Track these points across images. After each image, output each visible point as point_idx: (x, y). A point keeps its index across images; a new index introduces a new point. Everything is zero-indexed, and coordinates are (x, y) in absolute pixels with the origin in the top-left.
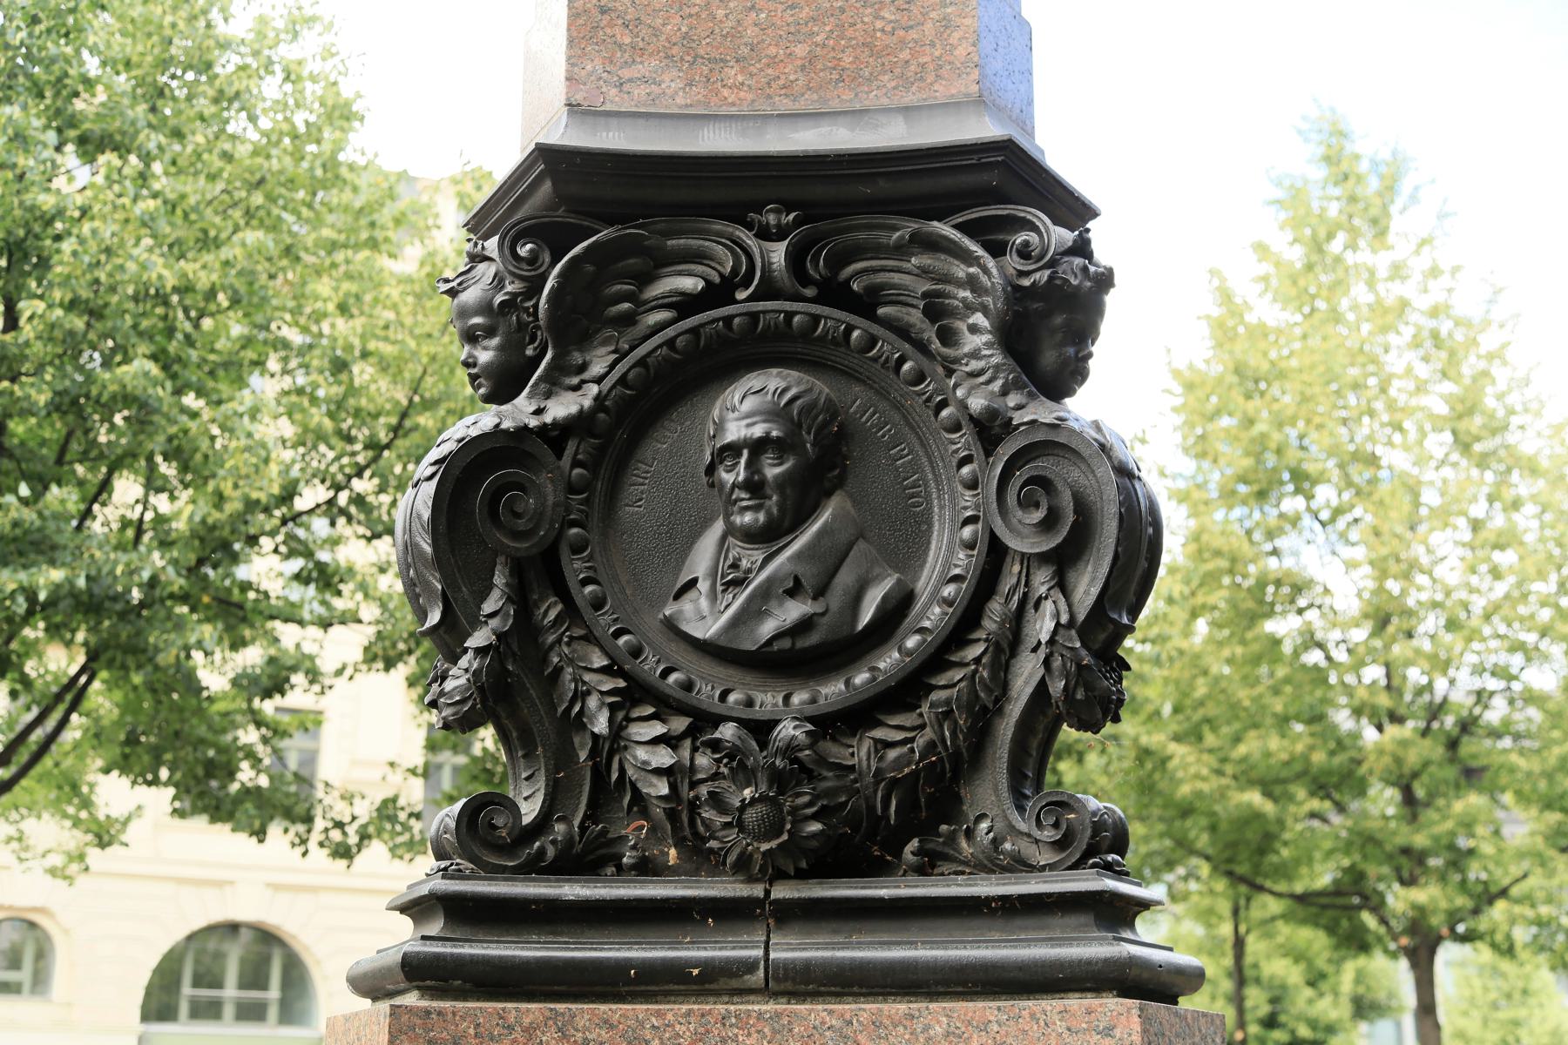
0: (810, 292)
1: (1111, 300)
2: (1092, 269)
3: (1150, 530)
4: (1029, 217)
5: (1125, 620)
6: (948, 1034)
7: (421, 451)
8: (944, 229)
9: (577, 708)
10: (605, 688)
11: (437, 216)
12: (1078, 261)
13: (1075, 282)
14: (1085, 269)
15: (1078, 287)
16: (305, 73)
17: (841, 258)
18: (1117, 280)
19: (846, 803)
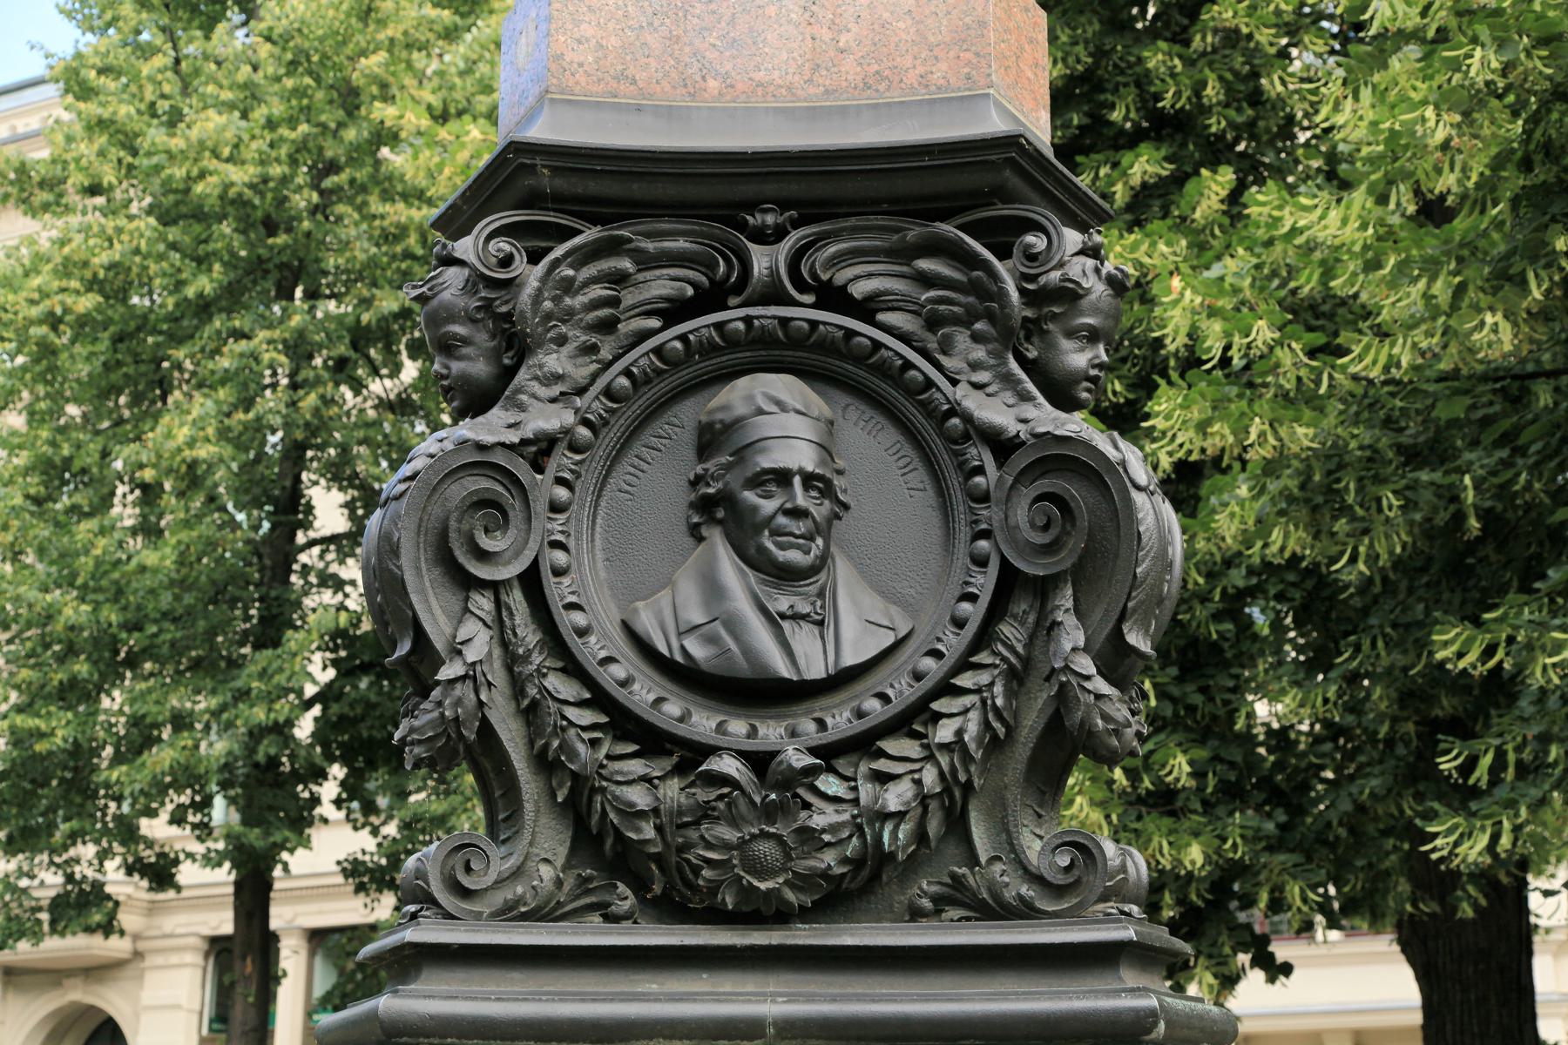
0: (809, 299)
9: (556, 743)
10: (584, 723)
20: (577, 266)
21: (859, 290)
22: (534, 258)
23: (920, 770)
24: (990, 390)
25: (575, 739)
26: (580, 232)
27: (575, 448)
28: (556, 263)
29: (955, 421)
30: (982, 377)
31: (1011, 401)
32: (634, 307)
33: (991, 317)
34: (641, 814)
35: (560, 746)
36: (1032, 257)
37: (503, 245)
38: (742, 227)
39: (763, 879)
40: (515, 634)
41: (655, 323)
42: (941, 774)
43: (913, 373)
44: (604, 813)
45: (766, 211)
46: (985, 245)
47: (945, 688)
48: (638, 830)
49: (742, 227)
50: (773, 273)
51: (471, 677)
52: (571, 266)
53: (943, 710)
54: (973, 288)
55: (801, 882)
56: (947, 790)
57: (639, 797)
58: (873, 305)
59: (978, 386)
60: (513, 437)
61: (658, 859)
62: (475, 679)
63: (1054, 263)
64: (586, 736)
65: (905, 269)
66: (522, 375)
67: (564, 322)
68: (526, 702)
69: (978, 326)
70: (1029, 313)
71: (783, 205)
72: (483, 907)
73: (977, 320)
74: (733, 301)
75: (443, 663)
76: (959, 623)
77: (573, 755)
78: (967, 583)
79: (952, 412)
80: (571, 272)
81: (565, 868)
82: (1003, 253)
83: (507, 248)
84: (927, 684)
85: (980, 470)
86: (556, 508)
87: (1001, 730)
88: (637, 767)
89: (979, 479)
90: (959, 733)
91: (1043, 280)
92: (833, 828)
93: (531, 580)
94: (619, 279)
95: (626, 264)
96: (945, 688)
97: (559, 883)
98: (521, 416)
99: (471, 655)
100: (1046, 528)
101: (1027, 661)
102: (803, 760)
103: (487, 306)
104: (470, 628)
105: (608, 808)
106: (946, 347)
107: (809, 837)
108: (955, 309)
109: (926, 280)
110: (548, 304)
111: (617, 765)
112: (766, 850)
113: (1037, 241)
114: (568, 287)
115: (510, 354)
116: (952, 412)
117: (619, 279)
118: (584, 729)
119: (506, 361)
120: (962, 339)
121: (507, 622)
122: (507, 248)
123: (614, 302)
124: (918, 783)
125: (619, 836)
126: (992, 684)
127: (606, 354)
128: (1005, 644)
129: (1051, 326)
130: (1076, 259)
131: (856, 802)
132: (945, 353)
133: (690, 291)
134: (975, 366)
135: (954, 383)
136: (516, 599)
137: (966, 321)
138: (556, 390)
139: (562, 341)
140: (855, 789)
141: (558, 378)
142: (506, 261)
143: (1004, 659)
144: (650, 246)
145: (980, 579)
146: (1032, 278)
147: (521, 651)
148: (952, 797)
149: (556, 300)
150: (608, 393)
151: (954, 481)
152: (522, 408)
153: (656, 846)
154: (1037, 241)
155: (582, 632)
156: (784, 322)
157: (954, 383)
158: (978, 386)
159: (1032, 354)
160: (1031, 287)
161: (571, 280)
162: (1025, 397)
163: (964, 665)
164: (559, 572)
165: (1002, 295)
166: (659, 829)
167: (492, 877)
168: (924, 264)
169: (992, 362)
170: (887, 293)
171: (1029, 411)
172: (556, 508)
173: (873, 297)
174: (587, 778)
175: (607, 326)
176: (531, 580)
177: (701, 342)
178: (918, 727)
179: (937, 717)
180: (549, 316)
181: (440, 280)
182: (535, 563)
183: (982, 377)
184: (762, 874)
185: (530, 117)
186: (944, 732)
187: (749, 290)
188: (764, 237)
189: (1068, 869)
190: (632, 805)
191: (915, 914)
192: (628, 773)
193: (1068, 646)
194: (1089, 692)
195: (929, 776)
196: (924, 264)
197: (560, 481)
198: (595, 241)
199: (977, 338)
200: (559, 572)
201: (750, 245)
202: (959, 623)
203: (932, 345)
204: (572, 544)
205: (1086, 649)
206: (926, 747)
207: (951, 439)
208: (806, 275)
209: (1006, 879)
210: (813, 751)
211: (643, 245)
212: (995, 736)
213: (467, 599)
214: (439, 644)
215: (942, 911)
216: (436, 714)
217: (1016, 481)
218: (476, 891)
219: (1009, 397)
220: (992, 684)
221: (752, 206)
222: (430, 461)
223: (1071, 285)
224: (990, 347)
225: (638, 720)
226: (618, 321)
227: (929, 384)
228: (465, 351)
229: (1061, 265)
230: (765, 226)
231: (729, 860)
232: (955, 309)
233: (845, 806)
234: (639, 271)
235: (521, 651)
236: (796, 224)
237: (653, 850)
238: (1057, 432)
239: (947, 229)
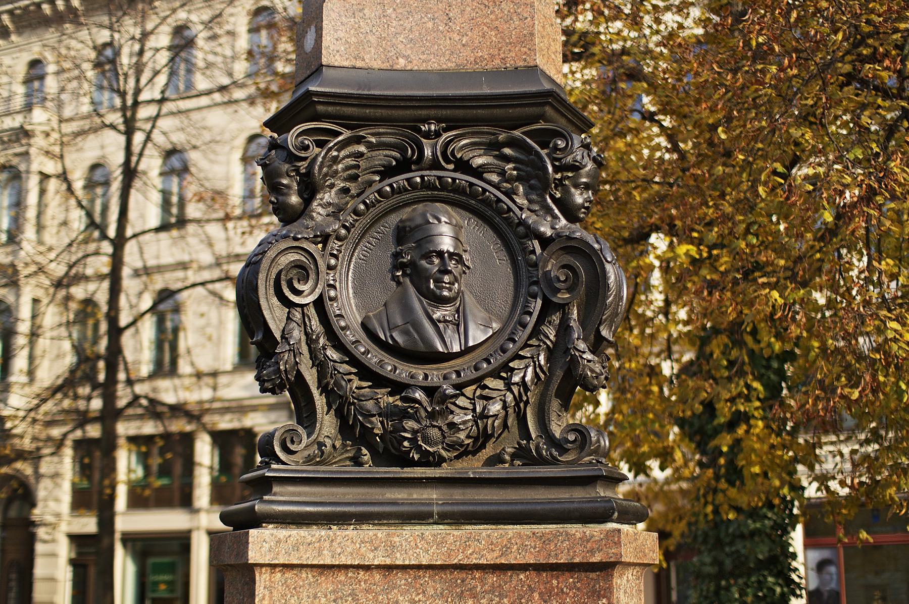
0: (451, 167)
20: (339, 150)
33: (537, 177)
38: (419, 131)
46: (535, 142)
52: (336, 150)
67: (333, 177)
69: (532, 182)
71: (439, 121)
113: (561, 144)
114: (335, 160)
123: (357, 167)
133: (394, 163)
154: (561, 144)
161: (338, 156)
180: (326, 175)
201: (422, 140)
221: (425, 121)
236: (446, 130)
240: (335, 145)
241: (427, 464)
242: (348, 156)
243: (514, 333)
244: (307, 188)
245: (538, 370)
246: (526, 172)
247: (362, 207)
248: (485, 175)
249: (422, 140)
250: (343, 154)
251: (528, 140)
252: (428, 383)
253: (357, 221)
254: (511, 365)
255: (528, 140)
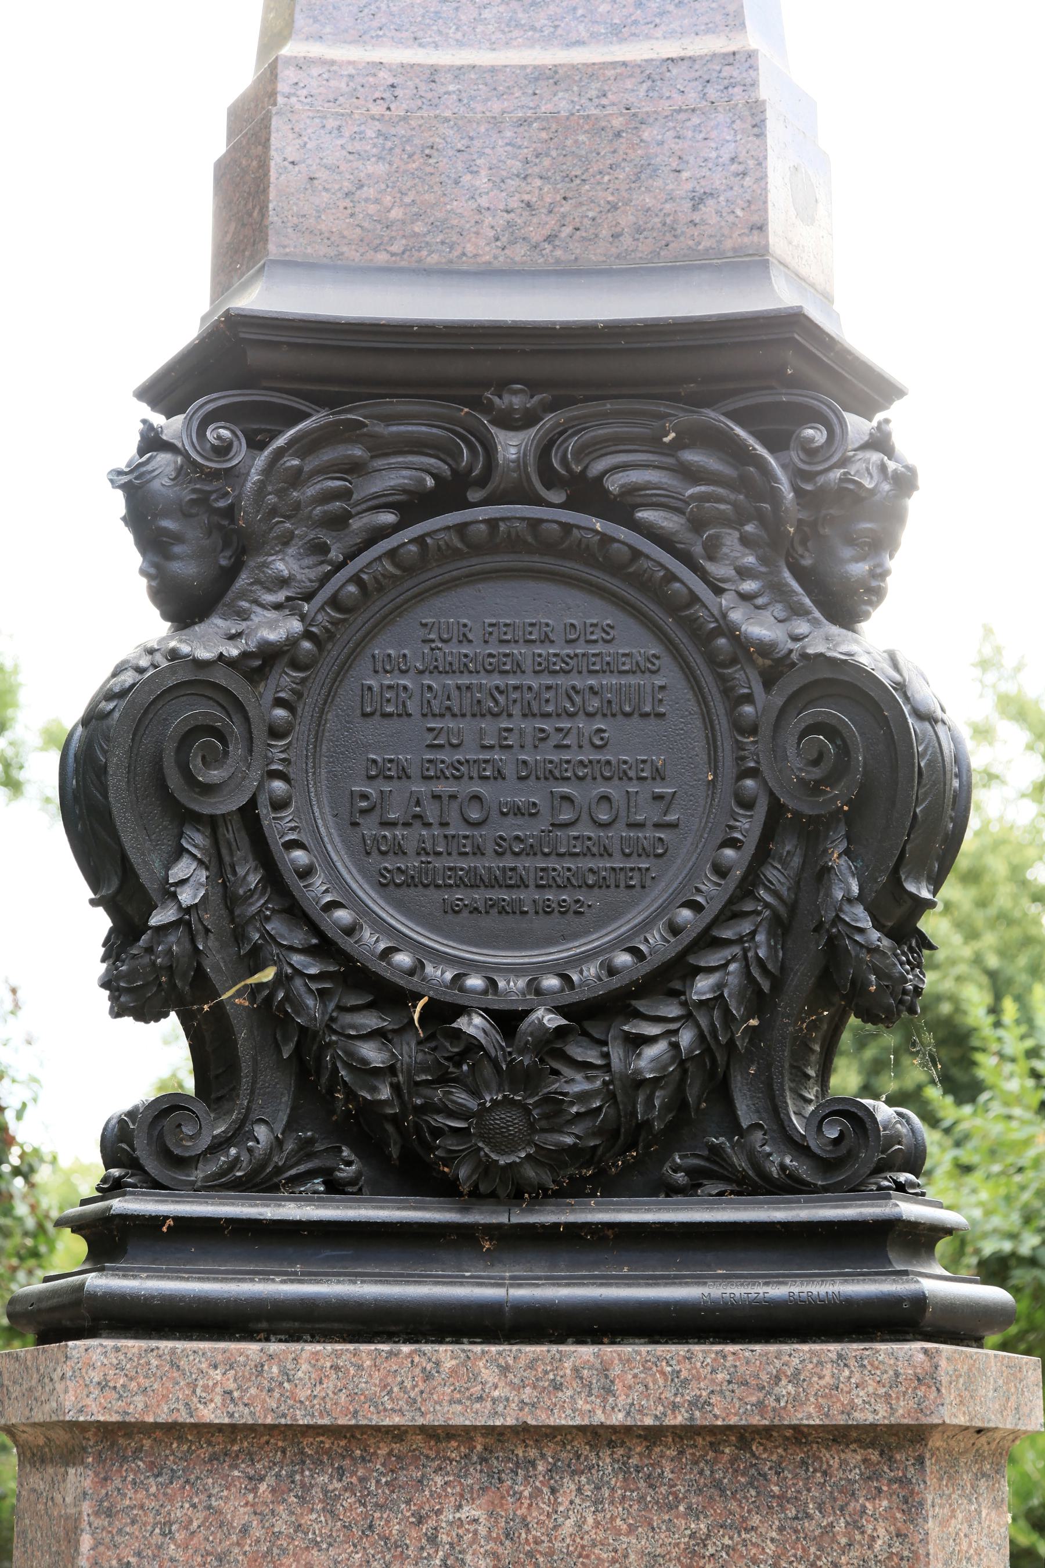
0: (557, 497)
1: (915, 505)
2: (891, 465)
3: (956, 783)
4: (801, 399)
5: (925, 894)
6: (848, 1563)
7: (158, 1434)
8: (713, 416)
9: (281, 995)
10: (313, 971)
11: (436, 46)
12: (875, 457)
13: (869, 484)
14: (883, 468)
15: (872, 492)
16: (672, 1399)
17: (589, 450)
18: (921, 481)
19: (600, 1108)
20: (302, 455)
21: (614, 484)
22: (256, 444)
23: (676, 1032)
24: (760, 601)
25: (302, 989)
26: (308, 416)
27: (296, 665)
28: (280, 453)
29: (722, 641)
30: (749, 586)
31: (782, 615)
32: (365, 500)
33: (761, 518)
34: (376, 1072)
35: (286, 998)
36: (811, 452)
37: (219, 433)
38: (487, 408)
39: (502, 1152)
40: (235, 873)
41: (388, 518)
42: (701, 1036)
43: (677, 585)
44: (335, 1070)
45: (515, 392)
46: (753, 434)
47: (707, 941)
48: (374, 1089)
49: (487, 408)
50: (520, 464)
51: (187, 920)
52: (296, 455)
53: (702, 964)
54: (742, 484)
55: (542, 1158)
56: (708, 1050)
57: (372, 1054)
58: (630, 500)
59: (746, 597)
60: (233, 651)
61: (395, 1119)
62: (188, 924)
63: (835, 459)
64: (314, 986)
65: (670, 460)
66: (243, 580)
67: (288, 518)
68: (247, 947)
69: (749, 528)
70: (803, 515)
71: (533, 386)
72: (198, 1175)
73: (748, 521)
74: (473, 496)
75: (156, 907)
76: (721, 871)
77: (300, 1008)
78: (731, 827)
79: (718, 632)
80: (296, 462)
81: (288, 1128)
82: (776, 443)
83: (225, 433)
84: (686, 939)
85: (749, 699)
86: (275, 732)
87: (766, 986)
88: (371, 1021)
89: (748, 709)
90: (720, 986)
91: (821, 480)
92: (583, 1097)
93: (249, 813)
94: (354, 468)
95: (357, 452)
96: (707, 941)
97: (279, 1143)
98: (242, 626)
99: (187, 897)
100: (816, 762)
101: (793, 908)
102: (552, 1021)
103: (203, 500)
104: (183, 869)
105: (339, 1065)
106: (712, 551)
107: (554, 1104)
108: (722, 507)
109: (691, 474)
110: (272, 499)
111: (348, 1018)
112: (508, 1120)
113: (816, 435)
114: (296, 478)
115: (228, 553)
116: (718, 632)
117: (354, 468)
118: (311, 977)
119: (224, 562)
120: (731, 540)
121: (227, 859)
122: (225, 433)
123: (345, 494)
124: (675, 1046)
125: (351, 1095)
126: (753, 933)
127: (335, 554)
128: (767, 889)
129: (827, 531)
130: (860, 455)
131: (607, 1067)
132: (711, 558)
133: (430, 482)
134: (744, 573)
135: (718, 591)
136: (234, 834)
137: (738, 521)
138: (280, 597)
139: (286, 540)
140: (606, 1056)
141: (283, 582)
142: (223, 450)
143: (767, 905)
144: (380, 429)
145: (744, 824)
146: (809, 477)
147: (241, 892)
148: (714, 1060)
149: (281, 493)
150: (334, 602)
151: (719, 707)
152: (244, 616)
153: (392, 1106)
154: (816, 435)
155: (306, 873)
156: (535, 524)
157: (718, 591)
158: (746, 597)
159: (807, 562)
160: (809, 487)
161: (299, 470)
162: (797, 611)
163: (730, 913)
164: (279, 805)
165: (775, 496)
166: (396, 1088)
167: (205, 1142)
168: (691, 456)
169: (763, 569)
170: (647, 486)
171: (802, 627)
172: (275, 732)
173: (631, 490)
174: (315, 1033)
175: (338, 522)
176: (249, 813)
177: (439, 548)
178: (677, 985)
179: (698, 970)
180: (274, 511)
181: (149, 467)
182: (253, 803)
183: (749, 586)
184: (508, 1145)
185: (61, 1209)
186: (703, 987)
187: (490, 487)
188: (509, 422)
189: (836, 1142)
190: (364, 1061)
191: (672, 1190)
192: (363, 1026)
193: (839, 895)
194: (861, 946)
195: (686, 1038)
196: (691, 456)
197: (280, 703)
198: (320, 428)
199: (746, 541)
200: (279, 805)
201: (493, 430)
202: (721, 871)
203: (698, 549)
204: (292, 772)
205: (860, 899)
206: (684, 1004)
207: (712, 660)
208: (556, 465)
209: (767, 1149)
210: (559, 1010)
211: (377, 429)
212: (759, 992)
213: (181, 835)
214: (151, 886)
215: (700, 1185)
216: (146, 960)
217: (803, 639)
218: (190, 1157)
219: (779, 610)
220: (753, 933)
221: (502, 385)
222: (138, 677)
223: (851, 486)
224: (760, 552)
225: (365, 970)
226: (350, 516)
227: (694, 599)
228: (177, 549)
229: (844, 462)
230: (511, 410)
231: (467, 1129)
232: (722, 507)
233: (594, 1073)
234: (372, 457)
235: (241, 892)
236: (552, 406)
237: (390, 1111)
238: (830, 654)
239: (713, 416)
240: (291, 443)
241: (492, 1198)
242: (323, 471)
243: (743, 759)
244: (226, 545)
245: (756, 973)
246: (734, 504)
247: (280, 713)
248: (251, 1325)
249: (493, 430)
250: (312, 463)
251: (739, 431)
252: (493, 1002)
253: (303, 681)
254: (692, 960)
255: (739, 431)
